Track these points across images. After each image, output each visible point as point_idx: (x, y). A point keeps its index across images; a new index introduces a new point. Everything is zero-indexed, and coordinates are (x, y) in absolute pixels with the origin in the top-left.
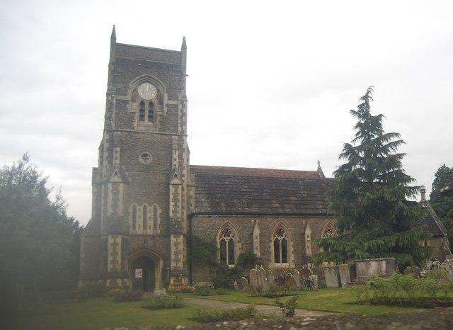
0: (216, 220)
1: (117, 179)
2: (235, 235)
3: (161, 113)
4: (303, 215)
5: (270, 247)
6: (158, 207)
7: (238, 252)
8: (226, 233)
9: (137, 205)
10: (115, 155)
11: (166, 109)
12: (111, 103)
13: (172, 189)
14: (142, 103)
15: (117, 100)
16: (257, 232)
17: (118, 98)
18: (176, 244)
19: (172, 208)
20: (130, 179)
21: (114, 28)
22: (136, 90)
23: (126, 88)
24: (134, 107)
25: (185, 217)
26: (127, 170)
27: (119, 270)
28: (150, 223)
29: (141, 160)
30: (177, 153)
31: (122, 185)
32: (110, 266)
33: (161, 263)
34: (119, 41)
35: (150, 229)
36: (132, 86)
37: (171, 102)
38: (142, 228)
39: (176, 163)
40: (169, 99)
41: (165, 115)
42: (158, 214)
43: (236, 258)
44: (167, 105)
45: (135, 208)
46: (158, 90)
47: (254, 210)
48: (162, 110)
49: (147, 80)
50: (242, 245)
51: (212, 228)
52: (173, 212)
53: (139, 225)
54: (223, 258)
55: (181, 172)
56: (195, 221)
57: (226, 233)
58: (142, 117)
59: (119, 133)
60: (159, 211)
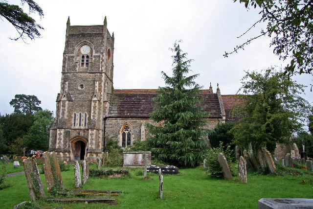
0: (120, 121)
1: (65, 99)
2: (132, 130)
4: (145, 117)
6: (87, 114)
7: (132, 140)
11: (94, 59)
13: (93, 104)
14: (83, 57)
18: (92, 134)
19: (92, 114)
20: (73, 99)
21: (69, 19)
22: (79, 50)
23: (74, 50)
24: (79, 59)
25: (101, 119)
28: (83, 123)
29: (79, 88)
30: (98, 82)
31: (67, 102)
34: (72, 24)
36: (77, 48)
37: (97, 54)
38: (78, 125)
39: (97, 88)
44: (94, 56)
45: (75, 115)
48: (92, 59)
56: (108, 122)
57: (127, 128)
58: (83, 64)
60: (88, 116)
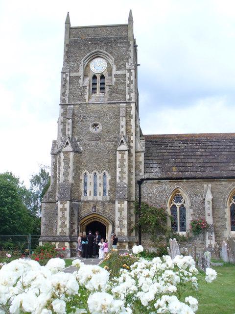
0: (168, 187)
3: (110, 84)
5: (225, 213)
6: (107, 174)
7: (189, 219)
8: (177, 197)
9: (97, 173)
10: (67, 127)
12: (65, 80)
13: (119, 156)
14: (95, 77)
15: (70, 77)
16: (209, 197)
17: (72, 75)
19: (118, 174)
21: (68, 15)
26: (79, 140)
27: (68, 234)
28: (100, 189)
29: (92, 130)
32: (59, 230)
33: (110, 227)
34: (72, 25)
35: (100, 195)
37: (119, 72)
38: (92, 194)
40: (118, 69)
41: (114, 85)
42: (108, 181)
43: (188, 226)
44: (116, 76)
45: (86, 175)
46: (108, 63)
47: (207, 174)
48: (111, 80)
49: (97, 55)
50: (194, 211)
51: (158, 194)
52: (120, 178)
53: (90, 191)
54: (174, 225)
55: (129, 138)
56: (145, 187)
59: (72, 106)
60: (109, 178)
